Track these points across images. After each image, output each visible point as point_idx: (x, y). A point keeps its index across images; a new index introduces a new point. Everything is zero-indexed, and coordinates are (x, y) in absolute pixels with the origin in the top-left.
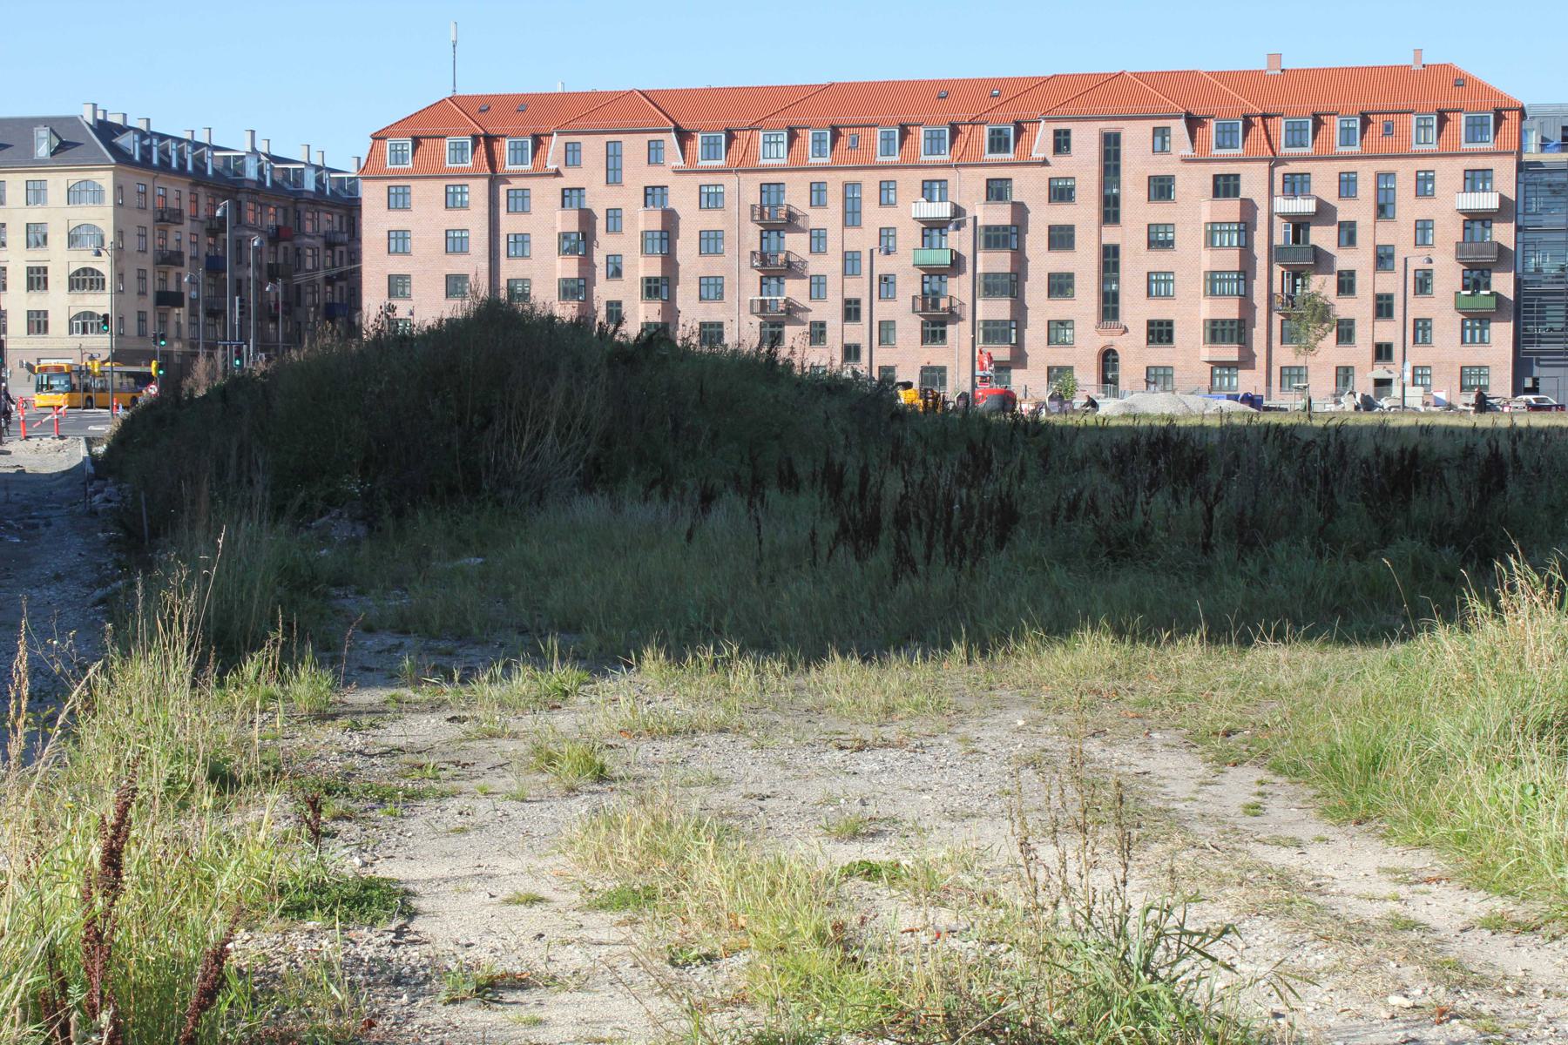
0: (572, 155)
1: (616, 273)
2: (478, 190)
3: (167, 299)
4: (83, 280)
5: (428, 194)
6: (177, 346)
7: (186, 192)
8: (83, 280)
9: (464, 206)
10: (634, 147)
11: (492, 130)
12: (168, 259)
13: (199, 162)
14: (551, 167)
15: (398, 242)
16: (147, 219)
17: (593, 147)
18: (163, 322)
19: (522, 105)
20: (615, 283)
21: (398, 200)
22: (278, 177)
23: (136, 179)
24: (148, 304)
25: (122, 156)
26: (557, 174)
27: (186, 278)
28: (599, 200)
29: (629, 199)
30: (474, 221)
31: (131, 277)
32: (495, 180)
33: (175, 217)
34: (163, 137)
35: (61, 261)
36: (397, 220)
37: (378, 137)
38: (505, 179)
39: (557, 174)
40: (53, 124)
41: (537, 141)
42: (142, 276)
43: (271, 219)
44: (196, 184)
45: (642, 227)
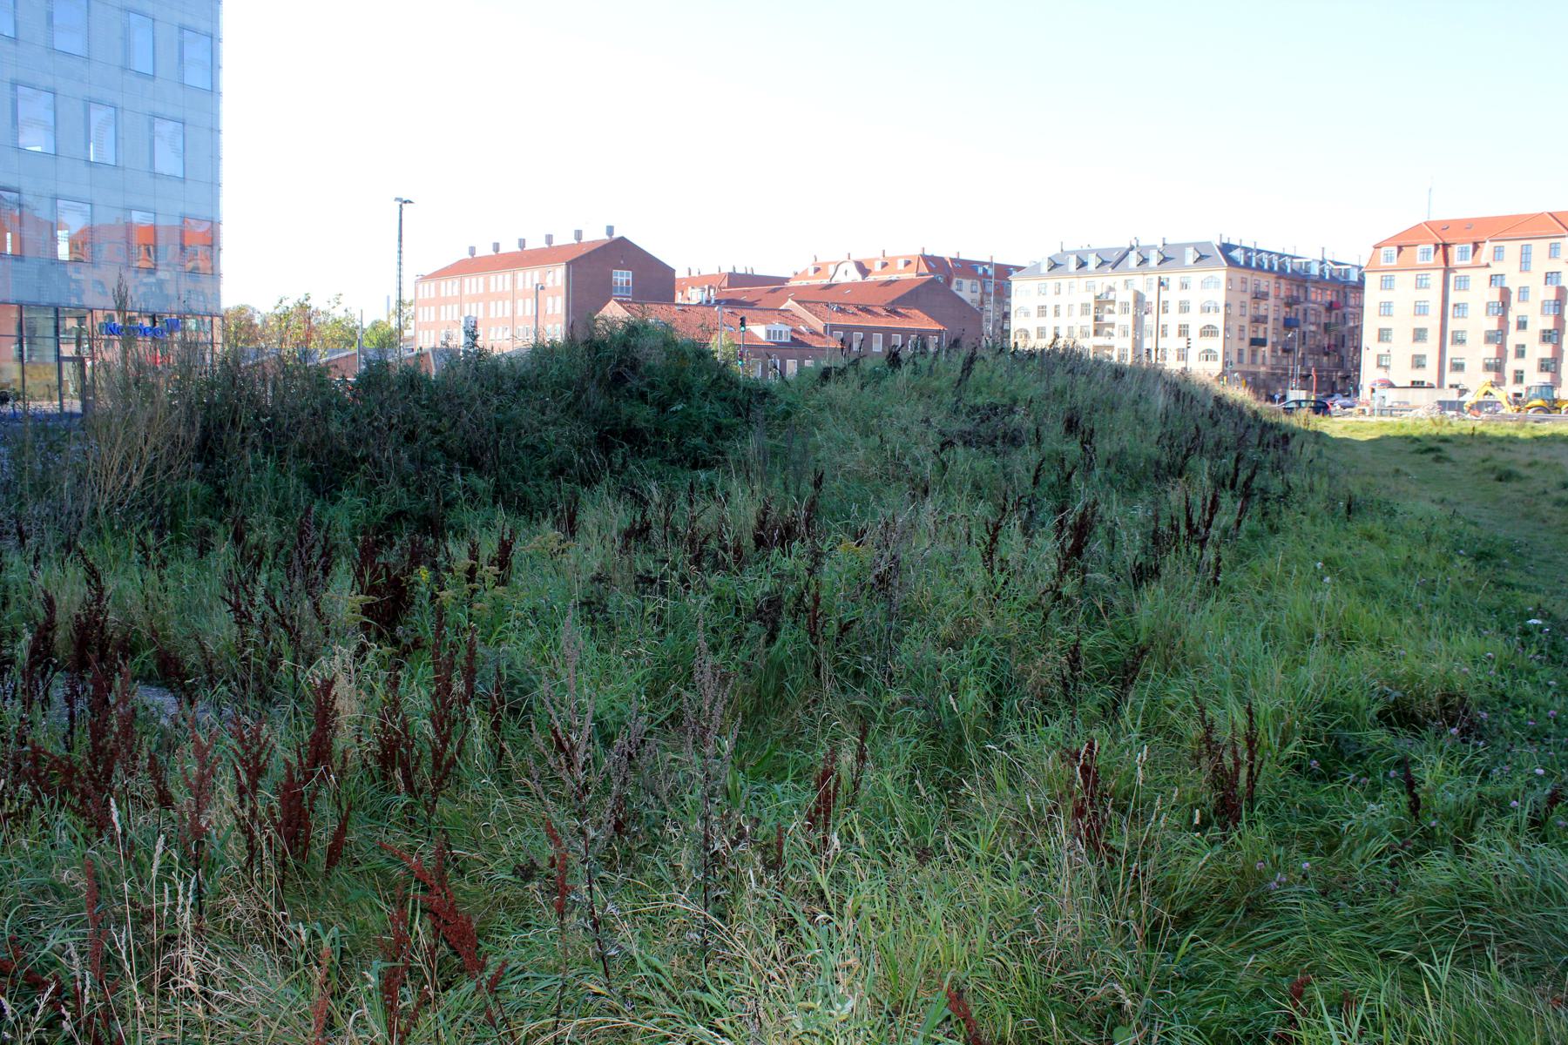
0: (1498, 254)
1: (1522, 325)
2: (1436, 277)
3: (1257, 342)
4: (1208, 331)
5: (1404, 280)
6: (1263, 369)
7: (1272, 282)
8: (1208, 331)
9: (1427, 287)
10: (1540, 248)
11: (1447, 241)
12: (1258, 320)
13: (1282, 268)
14: (1483, 261)
15: (1386, 308)
16: (1247, 298)
17: (1512, 249)
18: (1254, 354)
19: (1467, 225)
20: (1522, 333)
21: (1386, 284)
22: (1296, 267)
23: (1238, 274)
24: (1245, 345)
25: (1232, 262)
26: (1488, 266)
27: (1269, 332)
28: (1513, 282)
29: (1535, 281)
30: (1433, 297)
31: (1235, 330)
32: (1447, 271)
33: (1265, 296)
34: (1259, 252)
35: (1196, 321)
36: (1386, 296)
37: (1377, 247)
38: (1453, 270)
39: (1488, 266)
40: (1196, 247)
41: (1476, 246)
42: (1242, 329)
43: (1329, 296)
44: (1279, 277)
45: (1542, 297)
